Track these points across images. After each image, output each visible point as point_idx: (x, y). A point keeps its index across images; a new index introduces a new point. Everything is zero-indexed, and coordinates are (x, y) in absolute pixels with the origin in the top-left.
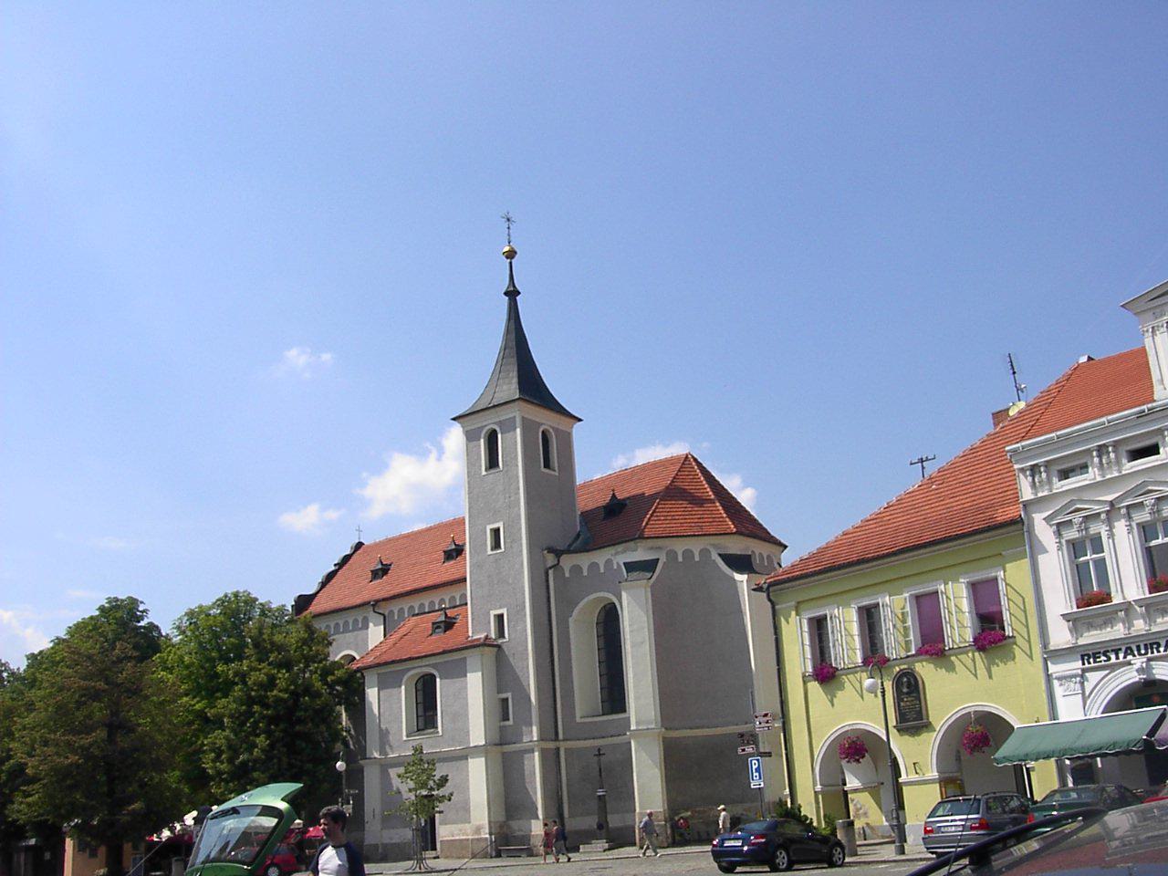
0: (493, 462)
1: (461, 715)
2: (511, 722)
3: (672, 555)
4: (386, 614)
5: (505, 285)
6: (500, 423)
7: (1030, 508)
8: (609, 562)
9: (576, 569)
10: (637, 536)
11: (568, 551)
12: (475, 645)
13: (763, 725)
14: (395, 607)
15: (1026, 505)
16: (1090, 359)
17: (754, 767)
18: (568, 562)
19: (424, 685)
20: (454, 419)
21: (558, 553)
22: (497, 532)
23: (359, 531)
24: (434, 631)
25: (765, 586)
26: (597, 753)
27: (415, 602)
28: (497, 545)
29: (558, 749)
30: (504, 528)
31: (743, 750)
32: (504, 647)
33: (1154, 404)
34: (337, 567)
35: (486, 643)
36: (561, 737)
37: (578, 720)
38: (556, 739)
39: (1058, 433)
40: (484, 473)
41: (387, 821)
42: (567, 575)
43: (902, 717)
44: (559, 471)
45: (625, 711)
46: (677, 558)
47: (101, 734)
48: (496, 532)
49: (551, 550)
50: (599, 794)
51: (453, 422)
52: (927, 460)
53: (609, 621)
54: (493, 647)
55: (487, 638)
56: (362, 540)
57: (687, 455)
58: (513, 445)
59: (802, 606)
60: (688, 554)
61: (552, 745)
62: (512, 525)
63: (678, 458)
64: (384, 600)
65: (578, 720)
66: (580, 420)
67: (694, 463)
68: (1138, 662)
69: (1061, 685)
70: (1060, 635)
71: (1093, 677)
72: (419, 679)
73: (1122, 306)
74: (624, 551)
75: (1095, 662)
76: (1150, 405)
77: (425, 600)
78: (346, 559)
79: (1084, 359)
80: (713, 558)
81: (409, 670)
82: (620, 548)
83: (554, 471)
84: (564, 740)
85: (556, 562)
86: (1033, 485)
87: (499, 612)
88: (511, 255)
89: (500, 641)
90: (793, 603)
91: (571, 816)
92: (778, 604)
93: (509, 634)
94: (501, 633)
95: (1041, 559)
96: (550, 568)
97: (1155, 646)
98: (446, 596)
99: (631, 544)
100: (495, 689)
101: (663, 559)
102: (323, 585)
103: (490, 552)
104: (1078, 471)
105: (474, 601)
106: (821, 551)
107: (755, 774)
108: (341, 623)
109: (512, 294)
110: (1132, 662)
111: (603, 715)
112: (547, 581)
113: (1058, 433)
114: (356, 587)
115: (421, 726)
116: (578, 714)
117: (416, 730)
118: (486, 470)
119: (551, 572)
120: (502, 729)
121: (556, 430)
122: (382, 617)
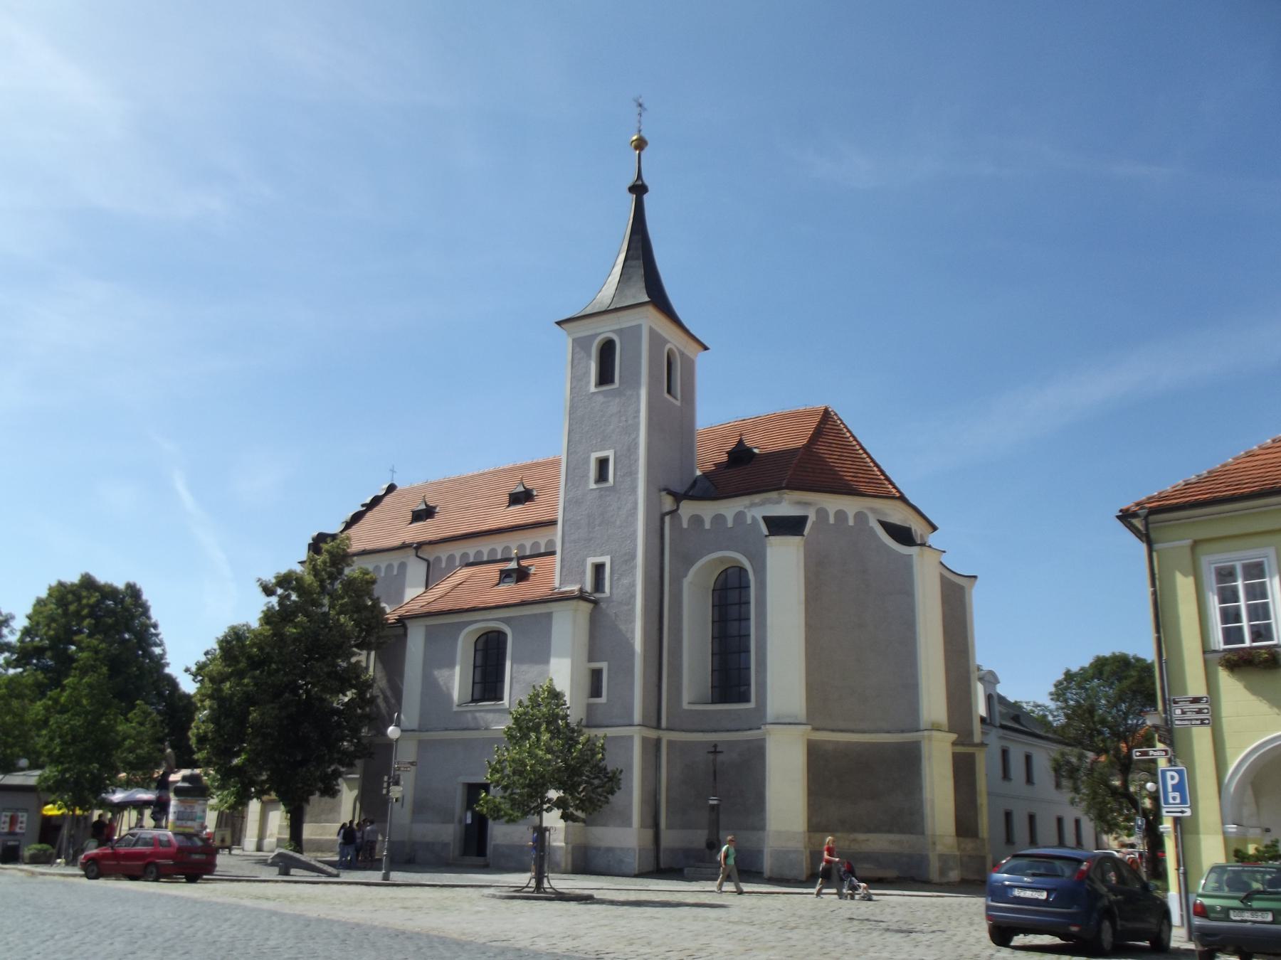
0: (605, 376)
2: (603, 700)
3: (822, 513)
4: (431, 559)
5: (631, 179)
6: (620, 332)
8: (740, 516)
9: (697, 520)
12: (565, 598)
14: (443, 552)
17: (1170, 783)
18: (688, 509)
19: (486, 642)
21: (678, 497)
22: (603, 463)
23: (393, 471)
24: (501, 581)
26: (713, 749)
27: (471, 548)
28: (602, 476)
29: (658, 742)
31: (1145, 754)
32: (603, 605)
34: (364, 508)
35: (582, 596)
36: (664, 723)
37: (685, 706)
38: (658, 727)
40: (593, 389)
41: (421, 807)
42: (685, 525)
45: (745, 698)
46: (827, 519)
47: (34, 716)
48: (603, 463)
49: (670, 493)
50: (711, 802)
55: (581, 590)
61: (653, 734)
63: (809, 414)
64: (431, 543)
65: (685, 706)
66: (706, 348)
72: (482, 635)
74: (763, 503)
77: (485, 547)
78: (376, 501)
80: (871, 525)
81: (476, 622)
82: (757, 498)
83: (675, 398)
84: (668, 729)
85: (675, 508)
87: (598, 560)
88: (640, 144)
89: (598, 595)
90: (1188, 542)
91: (669, 827)
92: (1157, 542)
93: (611, 588)
99: (774, 495)
103: (592, 486)
105: (567, 545)
106: (1212, 476)
107: (1171, 795)
109: (639, 189)
111: (713, 702)
112: (662, 529)
115: (477, 696)
116: (686, 697)
117: (470, 699)
119: (667, 519)
120: (590, 708)
121: (682, 354)
122: (423, 566)
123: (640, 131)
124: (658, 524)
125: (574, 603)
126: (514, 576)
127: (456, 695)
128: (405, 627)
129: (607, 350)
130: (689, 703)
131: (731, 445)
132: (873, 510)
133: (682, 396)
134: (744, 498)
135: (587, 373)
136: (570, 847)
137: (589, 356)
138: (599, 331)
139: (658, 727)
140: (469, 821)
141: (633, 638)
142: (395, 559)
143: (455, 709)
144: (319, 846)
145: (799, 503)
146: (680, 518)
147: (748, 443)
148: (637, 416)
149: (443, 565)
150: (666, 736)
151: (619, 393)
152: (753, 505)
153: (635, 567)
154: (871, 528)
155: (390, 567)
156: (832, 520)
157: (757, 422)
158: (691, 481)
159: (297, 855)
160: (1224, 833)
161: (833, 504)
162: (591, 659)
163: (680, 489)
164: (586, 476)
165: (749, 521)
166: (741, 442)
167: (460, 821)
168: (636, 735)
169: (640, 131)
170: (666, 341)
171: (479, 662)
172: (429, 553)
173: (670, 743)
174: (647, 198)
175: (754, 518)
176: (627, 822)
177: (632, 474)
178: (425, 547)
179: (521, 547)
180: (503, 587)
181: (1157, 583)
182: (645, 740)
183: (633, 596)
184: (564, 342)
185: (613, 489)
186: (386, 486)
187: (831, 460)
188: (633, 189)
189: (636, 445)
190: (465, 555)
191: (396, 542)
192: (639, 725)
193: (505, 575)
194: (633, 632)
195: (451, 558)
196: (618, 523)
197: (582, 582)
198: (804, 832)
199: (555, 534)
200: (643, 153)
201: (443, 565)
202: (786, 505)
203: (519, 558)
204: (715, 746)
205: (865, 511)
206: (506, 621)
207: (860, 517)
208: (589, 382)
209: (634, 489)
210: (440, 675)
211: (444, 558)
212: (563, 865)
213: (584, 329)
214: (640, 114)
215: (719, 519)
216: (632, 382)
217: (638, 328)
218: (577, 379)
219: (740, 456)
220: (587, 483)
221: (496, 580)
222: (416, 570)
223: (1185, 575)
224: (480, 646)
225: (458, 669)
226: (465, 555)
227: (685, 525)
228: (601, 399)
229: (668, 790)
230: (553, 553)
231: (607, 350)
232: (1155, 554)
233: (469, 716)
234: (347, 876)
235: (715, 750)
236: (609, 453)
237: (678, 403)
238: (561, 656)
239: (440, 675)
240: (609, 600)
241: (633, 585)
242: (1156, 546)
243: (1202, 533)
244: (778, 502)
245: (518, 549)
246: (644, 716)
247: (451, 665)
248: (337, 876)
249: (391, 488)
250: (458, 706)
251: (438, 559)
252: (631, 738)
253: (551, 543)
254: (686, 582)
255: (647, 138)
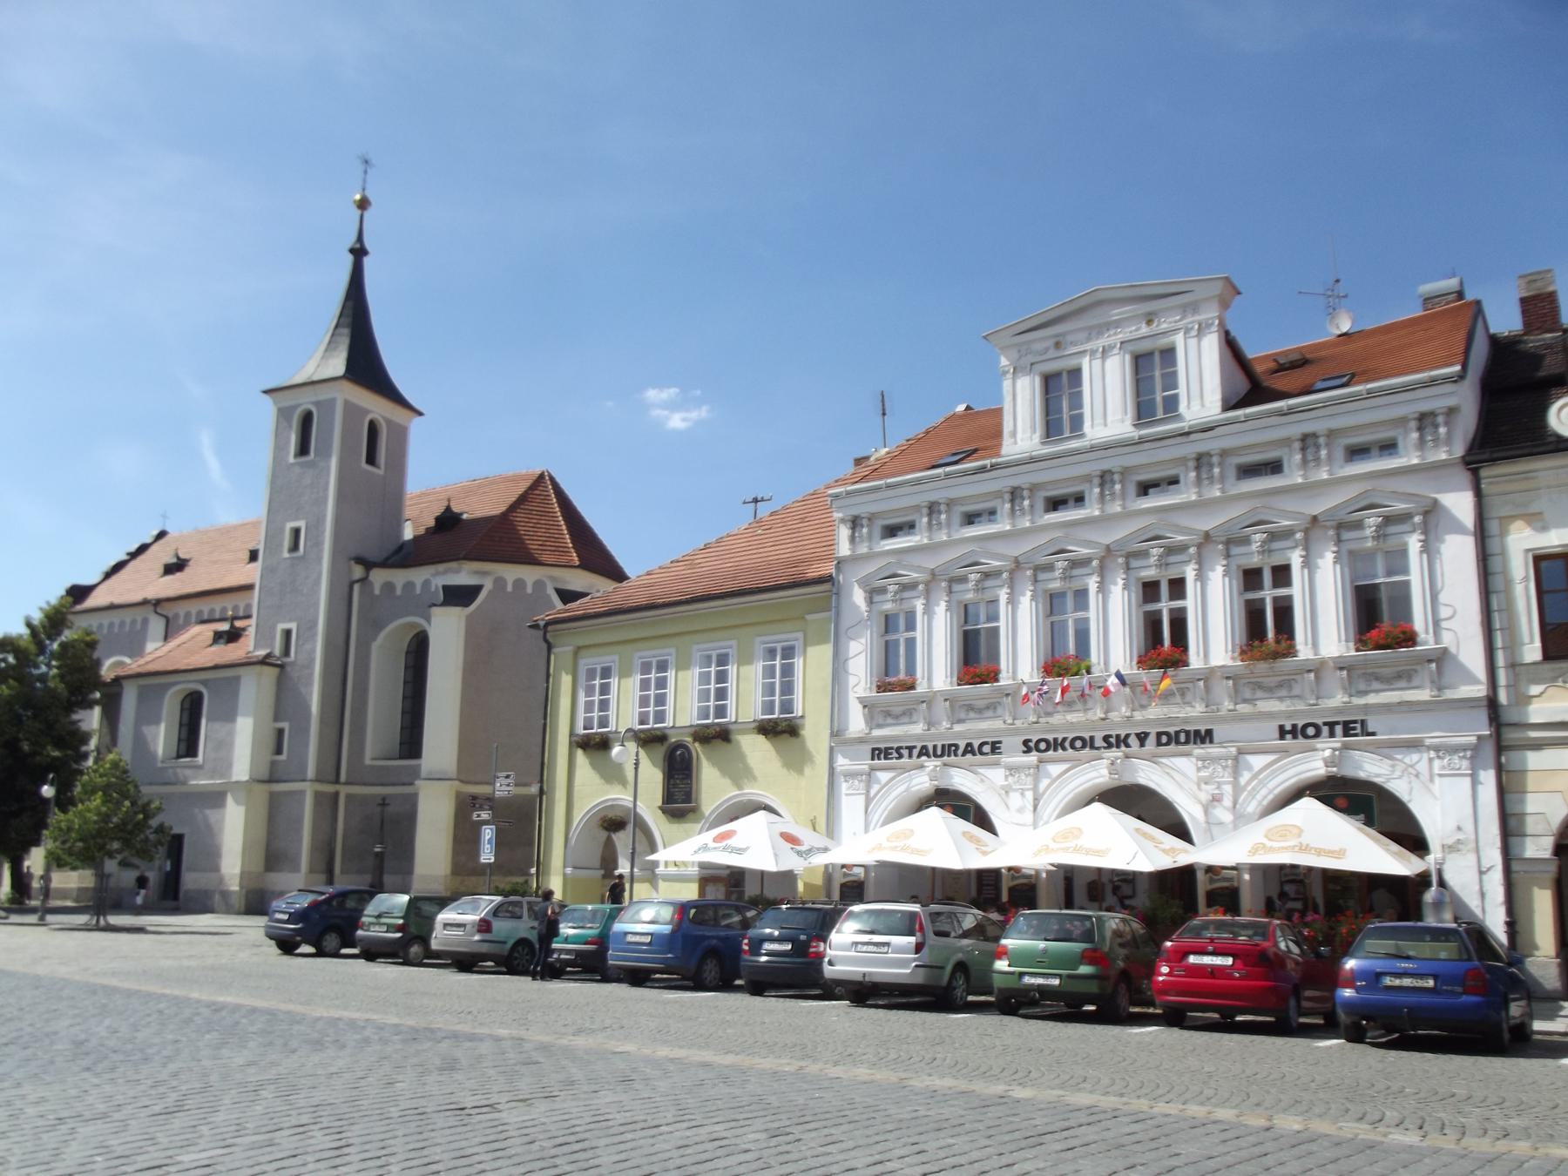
0: (303, 449)
1: (226, 745)
2: (283, 757)
3: (500, 583)
4: (170, 615)
5: (351, 240)
6: (318, 404)
7: (846, 567)
8: (426, 583)
9: (389, 587)
10: (461, 556)
11: (385, 564)
13: (504, 788)
14: (181, 609)
15: (840, 563)
16: (968, 408)
18: (379, 577)
20: (265, 392)
21: (368, 565)
22: (297, 532)
23: (164, 516)
25: (542, 623)
26: (381, 802)
27: (205, 606)
28: (295, 547)
29: (337, 794)
30: (307, 528)
32: (288, 669)
33: (1000, 460)
36: (343, 777)
37: (368, 762)
38: (337, 781)
39: (889, 481)
40: (291, 459)
42: (377, 592)
43: (669, 797)
44: (386, 468)
48: (297, 532)
49: (360, 560)
51: (264, 396)
52: (762, 500)
53: (418, 650)
54: (277, 664)
56: (168, 529)
57: (541, 476)
58: (334, 435)
59: (583, 653)
60: (519, 584)
61: (330, 788)
62: (316, 525)
64: (169, 600)
65: (368, 762)
66: (420, 414)
67: (549, 482)
68: (931, 764)
69: (846, 781)
70: (856, 723)
71: (883, 776)
72: (185, 697)
73: (985, 337)
74: (445, 572)
75: (886, 758)
76: (994, 461)
78: (143, 549)
79: (961, 408)
82: (441, 567)
84: (347, 783)
86: (852, 539)
88: (363, 204)
90: (570, 648)
93: (296, 653)
94: (286, 652)
95: (1480, 788)
96: (357, 581)
97: (953, 748)
98: (227, 604)
99: (453, 565)
100: (270, 714)
101: (488, 585)
102: (108, 575)
103: (286, 555)
104: (906, 530)
108: (139, 619)
109: (359, 252)
110: (926, 764)
111: (401, 757)
113: (889, 481)
114: (145, 582)
115: (182, 751)
117: (174, 755)
118: (296, 456)
119: (356, 587)
120: (273, 764)
121: (389, 422)
123: (364, 190)
124: (346, 589)
125: (258, 668)
126: (225, 637)
127: (160, 751)
128: (121, 686)
129: (307, 420)
130: (373, 759)
131: (438, 510)
132: (553, 579)
133: (386, 463)
134: (426, 567)
135: (288, 442)
136: (244, 891)
137: (290, 426)
138: (301, 401)
139: (337, 781)
140: (168, 868)
141: (311, 700)
142: (138, 614)
143: (159, 765)
144: (64, 894)
145: (476, 572)
146: (371, 584)
147: (456, 509)
148: (326, 489)
149: (181, 621)
150: (344, 790)
151: (312, 465)
152: (437, 574)
153: (315, 635)
154: (549, 596)
155: (134, 622)
156: (510, 588)
157: (468, 491)
158: (392, 547)
159: (1420, 924)
160: (565, 875)
161: (511, 573)
162: (276, 718)
163: (373, 554)
164: (281, 545)
165: (433, 589)
166: (448, 509)
167: (160, 869)
168: (309, 790)
169: (364, 190)
170: (367, 412)
171: (185, 720)
172: (169, 610)
173: (349, 797)
174: (367, 261)
175: (436, 586)
176: (296, 869)
177: (318, 544)
178: (165, 604)
179: (235, 608)
180: (214, 648)
181: (551, 680)
182: (318, 796)
183: (312, 660)
184: (268, 407)
185: (303, 558)
186: (155, 532)
187: (522, 530)
188: (352, 251)
189: (324, 516)
190: (200, 613)
191: (138, 598)
192: (311, 781)
193: (218, 637)
194: (311, 694)
195: (188, 615)
196: (305, 591)
197: (272, 646)
198: (446, 876)
199: (252, 598)
200: (367, 214)
201: (181, 621)
202: (463, 575)
203: (235, 618)
204: (384, 799)
205: (544, 579)
206: (204, 683)
207: (539, 585)
208: (288, 453)
209: (319, 560)
210: (147, 730)
211: (182, 614)
212: (237, 906)
213: (288, 399)
214: (366, 172)
215: (409, 586)
216: (325, 453)
217: (332, 402)
218: (279, 448)
219: (448, 521)
220: (281, 552)
221: (210, 642)
222: (157, 625)
223: (567, 674)
224: (187, 705)
225: (163, 727)
226: (200, 613)
227: (377, 592)
228: (297, 470)
229: (345, 837)
230: (249, 617)
231: (307, 420)
232: (552, 657)
233: (170, 771)
234: (14, 918)
235: (384, 802)
236: (302, 524)
237: (381, 472)
238: (245, 715)
239: (147, 730)
240: (293, 664)
241: (313, 651)
242: (555, 650)
243: (581, 643)
244: (458, 571)
245: (233, 611)
246: (319, 770)
247: (157, 722)
248: (6, 918)
249: (162, 535)
250: (163, 762)
251: (176, 616)
252: (302, 793)
253: (249, 606)
254: (376, 647)
255: (371, 198)
